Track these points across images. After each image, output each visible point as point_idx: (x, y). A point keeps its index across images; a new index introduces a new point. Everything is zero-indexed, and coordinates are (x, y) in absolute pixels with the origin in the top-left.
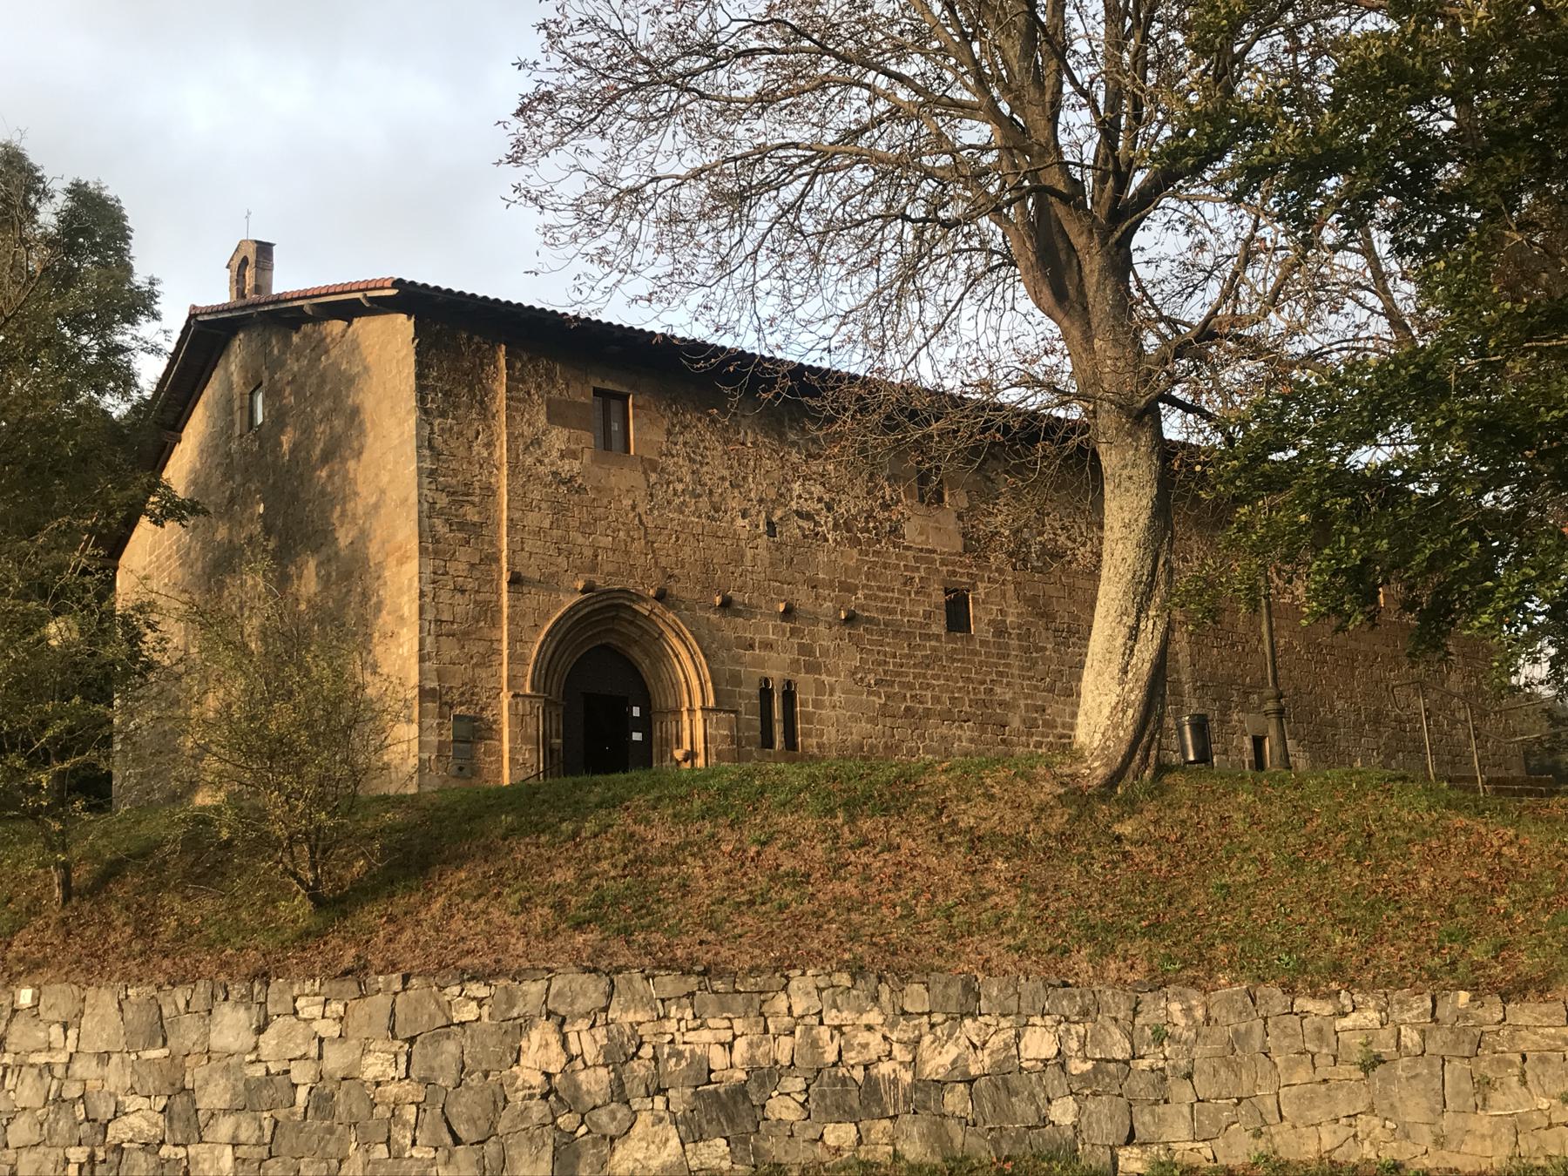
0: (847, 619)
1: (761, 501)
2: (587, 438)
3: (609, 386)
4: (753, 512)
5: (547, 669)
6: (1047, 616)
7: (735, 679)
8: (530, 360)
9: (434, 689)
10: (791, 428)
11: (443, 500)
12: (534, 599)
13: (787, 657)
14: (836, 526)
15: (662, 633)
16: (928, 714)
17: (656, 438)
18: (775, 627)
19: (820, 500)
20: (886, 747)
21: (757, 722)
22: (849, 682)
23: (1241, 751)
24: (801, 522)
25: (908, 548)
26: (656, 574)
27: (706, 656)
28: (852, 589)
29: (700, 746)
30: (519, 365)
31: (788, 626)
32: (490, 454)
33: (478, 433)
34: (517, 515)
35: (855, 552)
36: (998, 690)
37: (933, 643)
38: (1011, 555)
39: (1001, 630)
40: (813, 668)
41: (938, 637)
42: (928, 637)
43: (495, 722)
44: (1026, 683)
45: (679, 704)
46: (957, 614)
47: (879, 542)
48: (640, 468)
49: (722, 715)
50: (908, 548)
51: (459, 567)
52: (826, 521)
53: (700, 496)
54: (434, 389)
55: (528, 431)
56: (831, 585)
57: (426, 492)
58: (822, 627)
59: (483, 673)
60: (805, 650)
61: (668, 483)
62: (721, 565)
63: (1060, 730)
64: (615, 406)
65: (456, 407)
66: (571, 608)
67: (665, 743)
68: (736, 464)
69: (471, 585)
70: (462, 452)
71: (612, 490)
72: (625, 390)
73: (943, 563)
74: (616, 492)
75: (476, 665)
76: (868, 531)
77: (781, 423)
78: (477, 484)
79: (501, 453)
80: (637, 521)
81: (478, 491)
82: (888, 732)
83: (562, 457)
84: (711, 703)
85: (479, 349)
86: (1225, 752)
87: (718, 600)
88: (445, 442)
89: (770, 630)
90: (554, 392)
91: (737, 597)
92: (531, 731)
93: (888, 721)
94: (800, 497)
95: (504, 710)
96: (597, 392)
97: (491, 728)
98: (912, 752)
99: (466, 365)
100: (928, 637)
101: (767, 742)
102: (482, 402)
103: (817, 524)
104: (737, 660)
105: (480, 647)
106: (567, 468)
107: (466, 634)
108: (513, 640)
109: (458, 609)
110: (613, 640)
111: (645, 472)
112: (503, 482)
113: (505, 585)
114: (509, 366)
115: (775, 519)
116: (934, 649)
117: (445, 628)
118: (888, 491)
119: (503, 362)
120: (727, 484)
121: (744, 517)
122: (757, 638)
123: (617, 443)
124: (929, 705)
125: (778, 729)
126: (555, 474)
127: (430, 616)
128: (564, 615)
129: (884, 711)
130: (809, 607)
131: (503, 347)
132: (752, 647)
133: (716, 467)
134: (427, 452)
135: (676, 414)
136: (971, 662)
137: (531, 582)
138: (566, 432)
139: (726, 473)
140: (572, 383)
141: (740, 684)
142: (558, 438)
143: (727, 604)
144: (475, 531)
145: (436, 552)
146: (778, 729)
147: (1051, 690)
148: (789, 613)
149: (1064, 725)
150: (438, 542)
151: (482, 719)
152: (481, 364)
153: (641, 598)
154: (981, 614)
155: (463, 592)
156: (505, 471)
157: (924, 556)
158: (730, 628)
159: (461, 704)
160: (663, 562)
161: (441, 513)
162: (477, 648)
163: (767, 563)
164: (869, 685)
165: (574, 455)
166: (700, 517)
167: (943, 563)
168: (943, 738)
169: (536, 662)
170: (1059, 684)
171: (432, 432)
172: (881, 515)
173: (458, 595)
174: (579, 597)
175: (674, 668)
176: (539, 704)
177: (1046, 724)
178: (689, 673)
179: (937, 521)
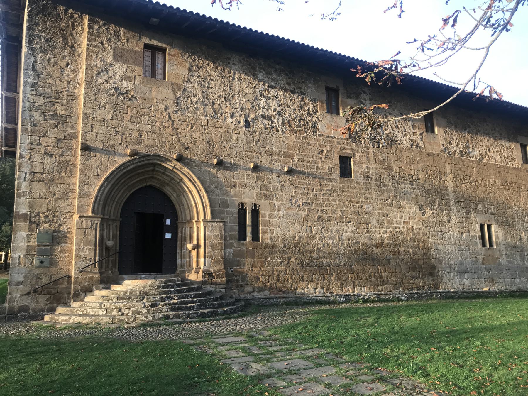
0: (217, 164)
1: (242, 109)
2: (138, 70)
3: (154, 42)
4: (237, 115)
5: (103, 203)
6: (389, 169)
7: (225, 204)
8: (104, 25)
9: (26, 214)
10: (260, 72)
11: (41, 101)
12: (96, 159)
13: (254, 192)
14: (283, 123)
15: (181, 180)
16: (329, 219)
17: (181, 73)
19: (275, 110)
20: (308, 237)
21: (237, 228)
22: (288, 204)
23: (475, 231)
24: (264, 121)
25: (321, 136)
26: (178, 146)
27: (207, 192)
28: (291, 156)
29: (202, 242)
30: (96, 27)
31: (255, 175)
32: (76, 76)
33: (68, 64)
34: (90, 111)
35: (293, 137)
36: (365, 206)
37: (333, 183)
38: (371, 140)
39: (367, 177)
40: (268, 197)
41: (335, 180)
42: (330, 180)
43: (69, 232)
44: (379, 202)
45: (191, 219)
46: (345, 163)
47: (306, 132)
48: (170, 88)
49: (215, 224)
50: (321, 136)
51: (49, 141)
52: (278, 122)
53: (206, 105)
54: (39, 37)
55: (100, 64)
56: (279, 154)
57: (28, 95)
58: (274, 175)
59: (62, 203)
60: (264, 187)
61: (188, 97)
62: (217, 142)
63: (395, 225)
64: (159, 57)
65: (54, 48)
66: (121, 166)
67: (184, 240)
68: (228, 89)
69: (57, 151)
70: (56, 74)
71: (153, 99)
72: (163, 45)
73: (339, 143)
74: (155, 101)
75: (58, 199)
76: (300, 126)
77: (254, 69)
78: (65, 93)
79: (82, 76)
80: (167, 117)
81: (65, 97)
82: (309, 230)
83: (122, 80)
84: (209, 217)
85: (72, 17)
86: (469, 232)
87: (215, 161)
88: (44, 67)
89: (245, 177)
90: (119, 43)
91: (227, 160)
92: (91, 238)
93: (309, 224)
94: (264, 108)
95: (73, 226)
96: (147, 46)
97: (66, 237)
98: (321, 240)
99: (63, 25)
100: (330, 180)
102: (72, 47)
103: (272, 122)
104: (226, 194)
105: (62, 188)
106: (124, 86)
107: (51, 180)
108: (83, 184)
109: (47, 166)
110: (154, 183)
111: (173, 90)
112: (81, 91)
113: (79, 152)
114: (90, 27)
115: (250, 119)
116: (333, 186)
118: (311, 107)
119: (86, 26)
120: (223, 99)
121: (232, 117)
122: (238, 182)
123: (159, 76)
124: (331, 215)
125: (249, 230)
126: (116, 89)
128: (117, 169)
129: (307, 219)
130: (268, 166)
131: (87, 16)
132: (234, 186)
133: (217, 88)
134: (31, 73)
135: (194, 61)
136: (351, 192)
137: (96, 150)
138: (125, 66)
139: (223, 93)
140: (131, 40)
141: (227, 206)
143: (220, 164)
144: (60, 121)
145: (33, 132)
146: (249, 230)
147: (391, 205)
148: (256, 168)
149: (397, 223)
150: (35, 125)
151: (59, 231)
152: (73, 25)
153: (167, 160)
154: (357, 169)
155: (51, 155)
156: (83, 86)
157: (329, 139)
158: (222, 176)
159: (45, 222)
160: (183, 140)
161: (38, 109)
162: (59, 189)
163: (244, 142)
164: (299, 205)
165: (129, 79)
166: (206, 116)
167: (339, 143)
168: (338, 231)
169: (97, 196)
170: (394, 202)
172: (309, 118)
173: (47, 158)
174: (128, 159)
175: (188, 196)
176: (98, 221)
177: (388, 222)
178: (197, 200)
179: (336, 122)
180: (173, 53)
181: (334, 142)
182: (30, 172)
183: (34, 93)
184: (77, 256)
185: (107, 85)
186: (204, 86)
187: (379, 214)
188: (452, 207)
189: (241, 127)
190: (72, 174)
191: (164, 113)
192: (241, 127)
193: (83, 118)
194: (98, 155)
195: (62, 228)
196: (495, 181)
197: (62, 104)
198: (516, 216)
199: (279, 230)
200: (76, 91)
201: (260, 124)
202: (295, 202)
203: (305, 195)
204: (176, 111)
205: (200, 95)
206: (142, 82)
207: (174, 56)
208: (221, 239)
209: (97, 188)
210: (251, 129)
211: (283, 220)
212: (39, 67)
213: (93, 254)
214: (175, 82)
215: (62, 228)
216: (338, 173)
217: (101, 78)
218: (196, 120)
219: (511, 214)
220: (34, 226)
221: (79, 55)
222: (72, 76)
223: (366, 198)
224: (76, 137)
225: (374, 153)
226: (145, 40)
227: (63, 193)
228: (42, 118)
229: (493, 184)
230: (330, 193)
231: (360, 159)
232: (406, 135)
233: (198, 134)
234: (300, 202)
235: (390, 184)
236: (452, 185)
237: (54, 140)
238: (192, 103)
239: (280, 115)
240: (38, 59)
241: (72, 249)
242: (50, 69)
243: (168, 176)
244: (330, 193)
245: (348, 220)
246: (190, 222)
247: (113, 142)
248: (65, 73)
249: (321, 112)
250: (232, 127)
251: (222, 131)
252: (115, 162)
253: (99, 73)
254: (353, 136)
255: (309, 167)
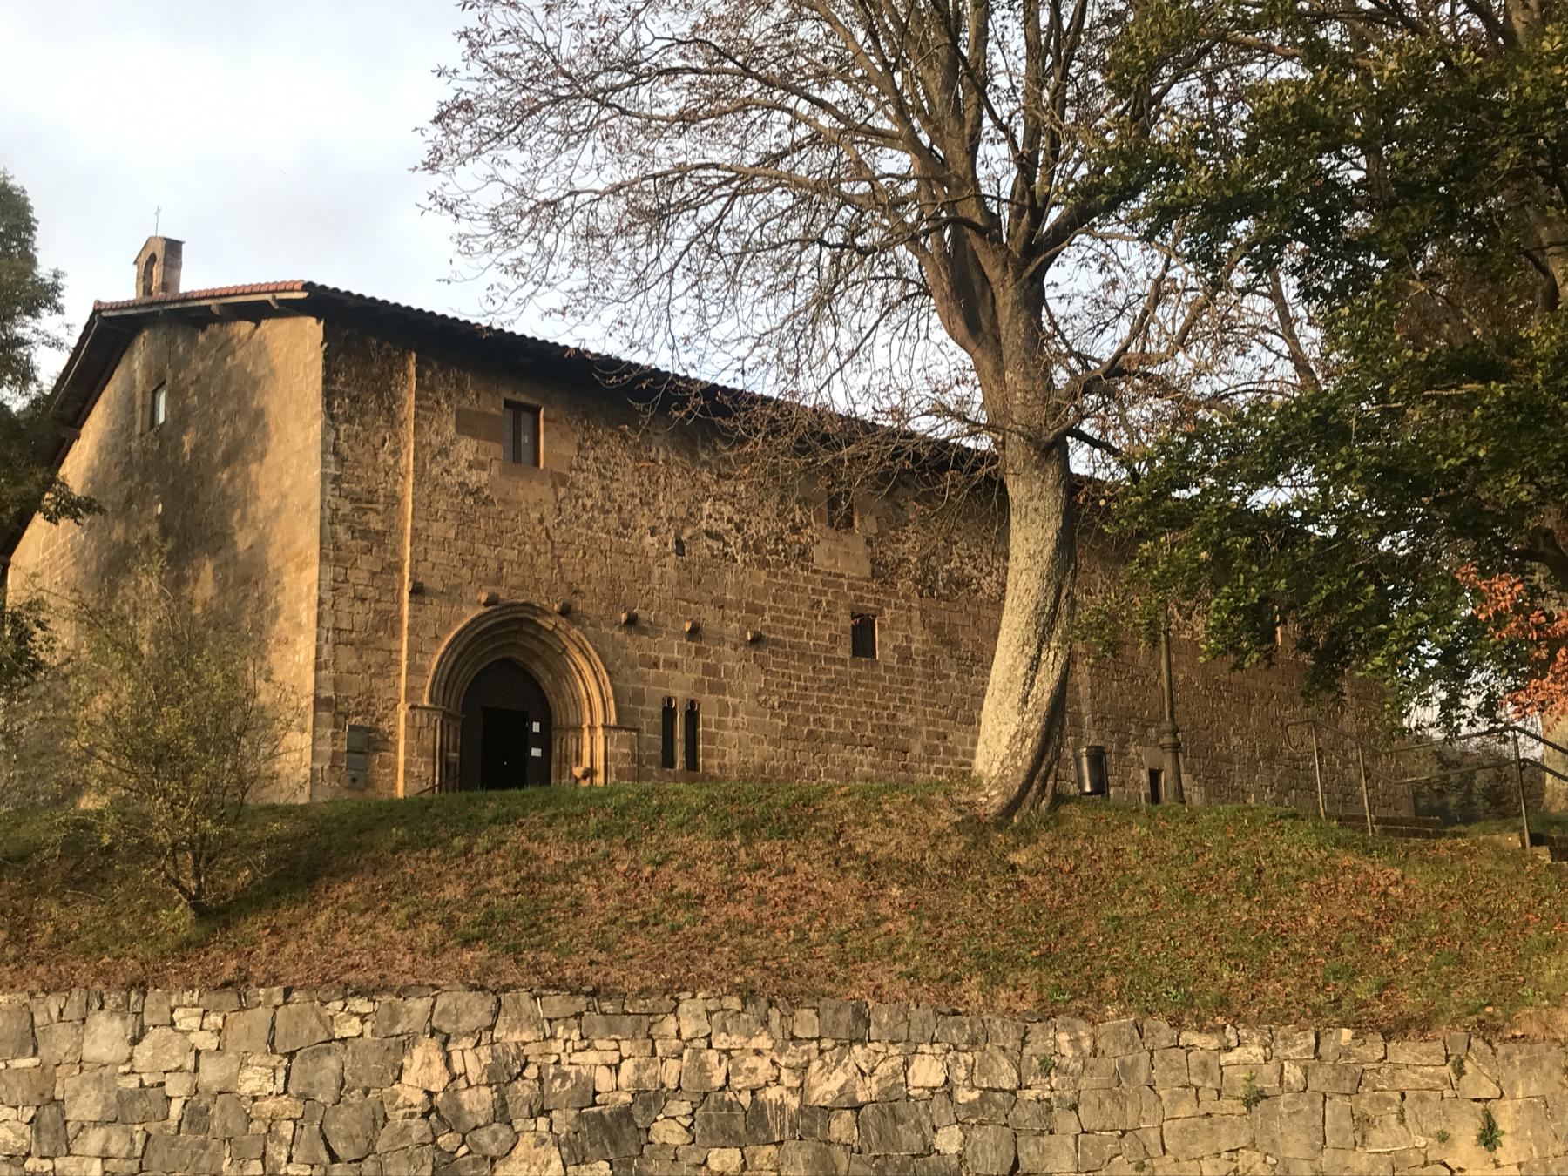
1: (671, 519)
3: (522, 398)
4: (663, 530)
5: (447, 681)
7: (638, 697)
8: (441, 368)
10: (704, 447)
11: (346, 507)
12: (435, 610)
13: (691, 677)
14: (745, 547)
15: (565, 649)
16: (830, 737)
18: (680, 645)
19: (730, 520)
20: (787, 769)
22: (753, 704)
23: (1137, 783)
24: (710, 542)
25: (816, 572)
26: (561, 589)
27: (609, 673)
29: (600, 764)
30: (429, 373)
31: (693, 645)
32: (396, 462)
35: (763, 574)
36: (900, 715)
37: (838, 667)
40: (717, 688)
41: (843, 662)
42: (834, 661)
43: (391, 733)
44: (928, 709)
46: (863, 639)
51: (360, 575)
52: (735, 542)
53: (608, 512)
54: (342, 394)
56: (738, 607)
57: (328, 498)
59: (380, 684)
60: (709, 670)
63: (960, 758)
64: (526, 419)
65: (363, 413)
66: (473, 621)
69: (372, 593)
70: (367, 459)
72: (535, 402)
73: (851, 587)
75: (373, 675)
77: (693, 441)
78: (381, 492)
79: (408, 461)
82: (790, 756)
83: (470, 467)
84: (613, 721)
85: (388, 355)
86: (1122, 784)
87: (624, 617)
91: (643, 615)
92: (428, 743)
93: (791, 744)
94: (710, 516)
96: (508, 403)
97: (386, 740)
98: (813, 776)
99: (375, 371)
100: (834, 661)
101: (668, 761)
102: (390, 409)
103: (726, 544)
104: (641, 678)
106: (474, 479)
107: (364, 643)
111: (554, 486)
113: (406, 595)
114: (419, 374)
115: (684, 538)
116: (838, 673)
117: (343, 636)
118: (798, 514)
119: (412, 370)
121: (652, 534)
122: (662, 656)
125: (680, 749)
127: (328, 624)
129: (787, 735)
132: (656, 665)
133: (627, 483)
134: (331, 458)
135: (587, 429)
136: (874, 686)
137: (433, 593)
139: (637, 490)
141: (643, 702)
142: (467, 449)
144: (378, 540)
145: (337, 560)
146: (680, 749)
147: (953, 718)
148: (695, 633)
149: (964, 753)
150: (339, 549)
151: (377, 730)
153: (544, 612)
154: (886, 640)
155: (363, 600)
156: (411, 479)
158: (634, 646)
159: (357, 714)
160: (569, 577)
161: (344, 520)
163: (674, 581)
165: (482, 466)
167: (851, 587)
168: (846, 762)
169: (436, 673)
171: (337, 438)
174: (482, 610)
176: (437, 717)
177: (947, 750)
178: (590, 690)
180: (553, 416)
181: (841, 585)
182: (335, 629)
183: (337, 493)
184: (407, 772)
185: (448, 479)
186: (605, 477)
187: (928, 732)
188: (1085, 730)
189: (669, 554)
190: (395, 634)
191: (538, 529)
192: (669, 554)
193: (412, 537)
194: (435, 601)
195: (381, 725)
196: (1189, 678)
197: (378, 513)
198: (1236, 757)
199: (735, 751)
200: (398, 488)
201: (703, 548)
202: (766, 701)
203: (784, 687)
204: (559, 524)
205: (597, 494)
206: (502, 472)
207: (553, 421)
208: (633, 761)
209: (437, 659)
210: (686, 558)
211: (741, 733)
212: (343, 447)
213: (430, 772)
214: (555, 469)
215: (381, 725)
216: (849, 647)
217: (438, 464)
218: (592, 540)
219: (1225, 752)
220: (341, 718)
221: (401, 425)
222: (391, 462)
223: (903, 700)
224: (399, 570)
225: (923, 610)
226: (507, 394)
227: (381, 667)
228: (349, 537)
229: (1184, 685)
230: (830, 687)
231: (893, 620)
232: (990, 574)
233: (595, 566)
234: (775, 701)
235: (953, 674)
236: (1088, 682)
237: (367, 575)
238: (584, 507)
239: (738, 530)
240: (342, 434)
241: (396, 763)
242: (359, 450)
243: (543, 642)
244: (830, 687)
245: (865, 740)
246: (578, 729)
247: (458, 580)
248: (381, 456)
249: (816, 529)
250: (652, 554)
251: (636, 560)
252: (461, 616)
253: (434, 457)
254: (882, 572)
255: (791, 633)
